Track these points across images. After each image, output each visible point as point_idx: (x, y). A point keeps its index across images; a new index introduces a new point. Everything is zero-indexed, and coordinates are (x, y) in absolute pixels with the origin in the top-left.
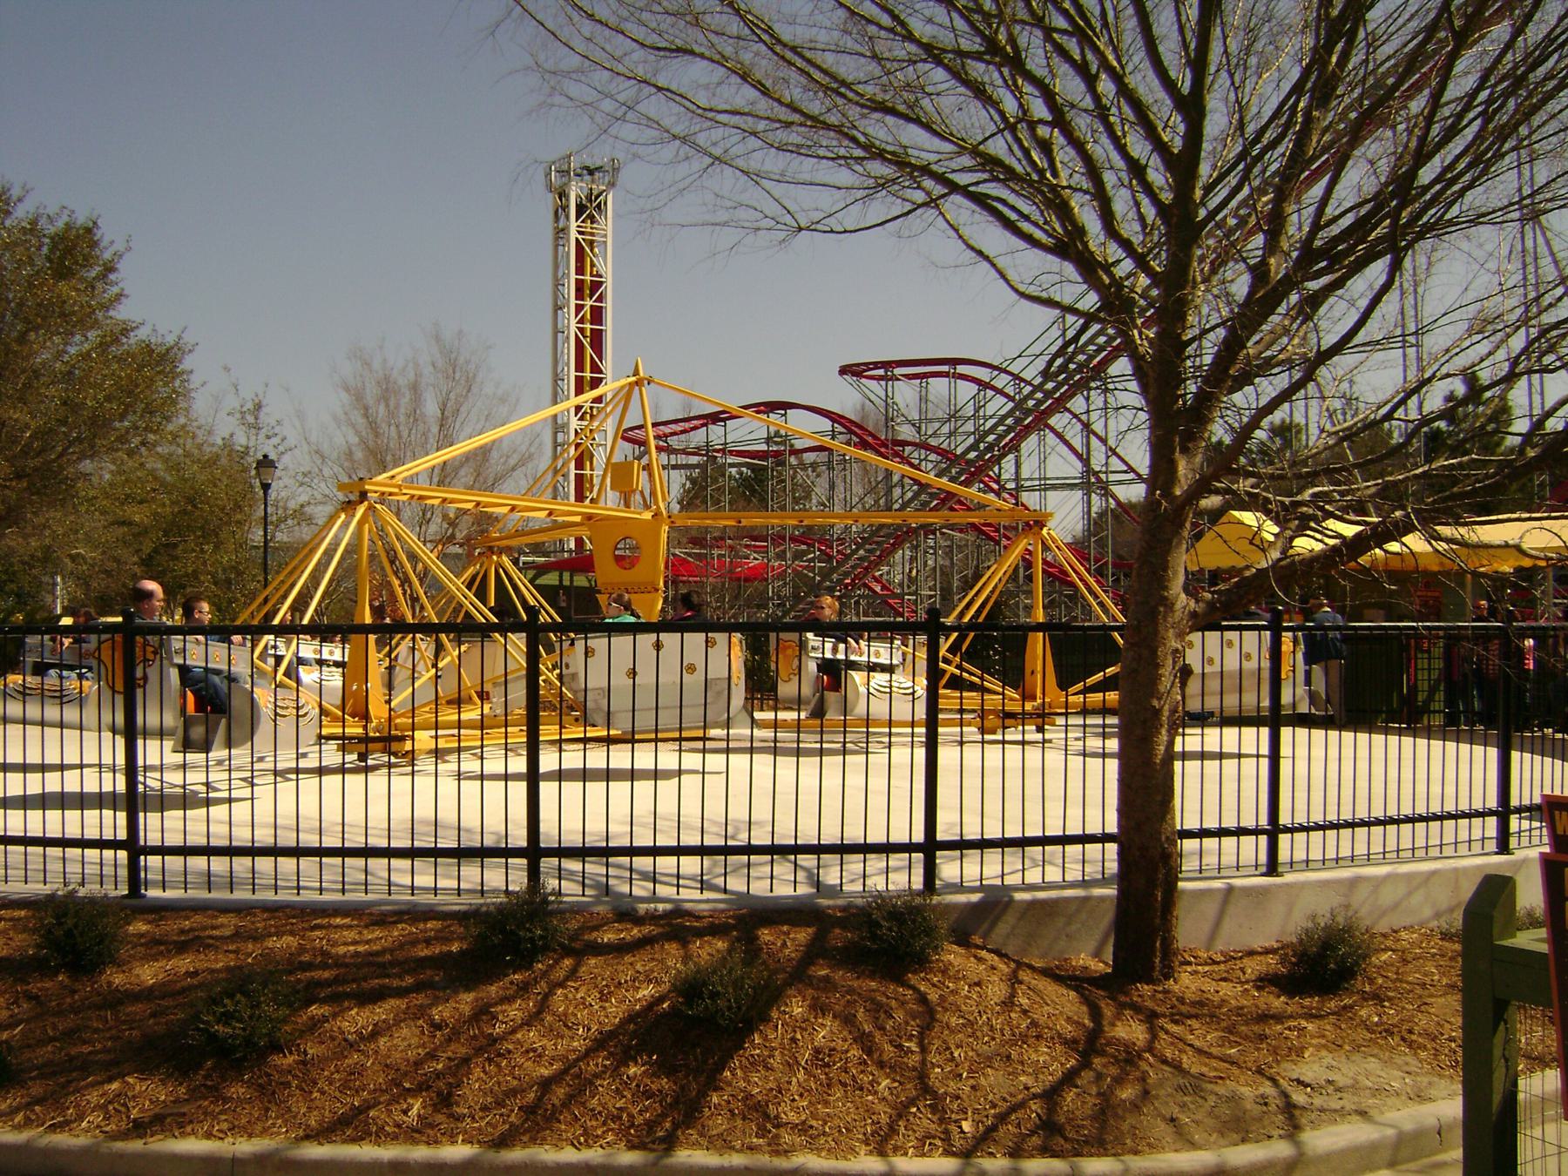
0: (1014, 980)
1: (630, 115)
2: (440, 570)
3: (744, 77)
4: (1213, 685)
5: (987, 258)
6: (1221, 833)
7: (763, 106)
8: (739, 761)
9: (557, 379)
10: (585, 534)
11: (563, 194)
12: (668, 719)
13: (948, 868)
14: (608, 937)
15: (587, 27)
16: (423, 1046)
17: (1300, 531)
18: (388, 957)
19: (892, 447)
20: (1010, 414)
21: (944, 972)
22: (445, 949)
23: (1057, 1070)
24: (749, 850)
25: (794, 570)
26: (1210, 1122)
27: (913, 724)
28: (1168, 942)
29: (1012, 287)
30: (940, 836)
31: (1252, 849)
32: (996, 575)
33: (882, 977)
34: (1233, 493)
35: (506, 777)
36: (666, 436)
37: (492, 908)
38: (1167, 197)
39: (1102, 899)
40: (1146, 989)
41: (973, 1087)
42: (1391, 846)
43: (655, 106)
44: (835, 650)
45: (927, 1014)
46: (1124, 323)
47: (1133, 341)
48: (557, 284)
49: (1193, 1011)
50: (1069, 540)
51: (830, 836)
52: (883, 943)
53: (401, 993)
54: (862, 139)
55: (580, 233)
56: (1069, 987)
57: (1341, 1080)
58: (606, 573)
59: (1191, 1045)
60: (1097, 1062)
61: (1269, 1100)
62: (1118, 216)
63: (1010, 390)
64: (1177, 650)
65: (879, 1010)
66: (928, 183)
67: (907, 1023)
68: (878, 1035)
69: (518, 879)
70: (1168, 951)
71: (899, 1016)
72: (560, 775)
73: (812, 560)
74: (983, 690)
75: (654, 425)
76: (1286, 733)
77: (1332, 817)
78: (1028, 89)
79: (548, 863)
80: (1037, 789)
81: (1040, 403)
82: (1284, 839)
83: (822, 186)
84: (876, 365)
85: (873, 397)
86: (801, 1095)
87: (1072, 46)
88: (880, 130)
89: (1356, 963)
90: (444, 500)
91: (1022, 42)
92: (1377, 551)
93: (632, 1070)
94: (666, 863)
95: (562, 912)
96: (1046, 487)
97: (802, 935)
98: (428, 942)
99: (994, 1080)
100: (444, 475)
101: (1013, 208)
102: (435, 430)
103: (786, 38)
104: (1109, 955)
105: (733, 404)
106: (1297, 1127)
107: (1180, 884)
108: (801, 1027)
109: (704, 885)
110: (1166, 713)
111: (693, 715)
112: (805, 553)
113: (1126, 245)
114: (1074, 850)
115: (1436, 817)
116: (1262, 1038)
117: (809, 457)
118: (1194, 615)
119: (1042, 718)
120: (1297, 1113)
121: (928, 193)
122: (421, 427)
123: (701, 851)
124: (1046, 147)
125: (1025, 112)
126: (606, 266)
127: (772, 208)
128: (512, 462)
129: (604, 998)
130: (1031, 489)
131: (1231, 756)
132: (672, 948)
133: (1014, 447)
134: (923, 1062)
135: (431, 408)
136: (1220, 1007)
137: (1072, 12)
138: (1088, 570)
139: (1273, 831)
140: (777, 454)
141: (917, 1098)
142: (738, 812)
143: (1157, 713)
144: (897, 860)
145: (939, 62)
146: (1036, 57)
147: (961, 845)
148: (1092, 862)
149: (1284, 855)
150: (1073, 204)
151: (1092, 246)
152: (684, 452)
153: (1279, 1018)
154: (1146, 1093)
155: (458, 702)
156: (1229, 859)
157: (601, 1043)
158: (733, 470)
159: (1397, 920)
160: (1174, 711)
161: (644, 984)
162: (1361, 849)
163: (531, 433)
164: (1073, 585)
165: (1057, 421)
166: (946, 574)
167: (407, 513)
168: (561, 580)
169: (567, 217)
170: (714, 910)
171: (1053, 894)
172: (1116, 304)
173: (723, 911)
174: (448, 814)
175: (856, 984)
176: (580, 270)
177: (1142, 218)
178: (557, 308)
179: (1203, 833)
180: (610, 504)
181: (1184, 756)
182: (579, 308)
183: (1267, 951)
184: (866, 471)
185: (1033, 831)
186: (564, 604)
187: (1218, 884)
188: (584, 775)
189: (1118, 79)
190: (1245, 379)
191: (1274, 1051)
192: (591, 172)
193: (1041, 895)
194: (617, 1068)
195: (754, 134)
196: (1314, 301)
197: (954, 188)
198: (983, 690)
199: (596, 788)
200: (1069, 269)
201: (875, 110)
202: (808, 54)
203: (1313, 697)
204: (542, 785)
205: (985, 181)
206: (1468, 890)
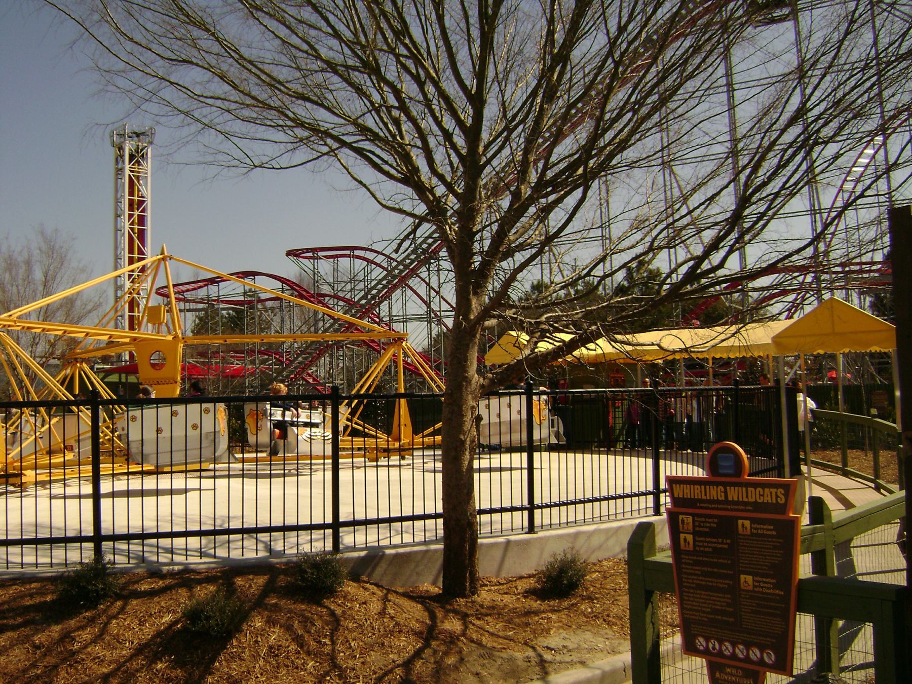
0: (385, 600)
1: (154, 99)
2: (42, 373)
3: (222, 77)
4: (505, 428)
5: (365, 186)
6: (502, 510)
7: (234, 95)
8: (222, 483)
9: (117, 258)
10: (133, 349)
11: (121, 148)
12: (179, 457)
13: (347, 538)
14: (144, 587)
15: (129, 46)
16: (28, 660)
17: (542, 338)
18: (6, 606)
19: (319, 298)
20: (384, 278)
21: (345, 597)
22: (42, 599)
23: (411, 650)
24: (229, 532)
25: (261, 371)
26: (498, 673)
27: (324, 458)
28: (473, 574)
29: (378, 202)
30: (342, 519)
31: (520, 519)
32: (377, 369)
33: (309, 603)
34: (503, 317)
35: (80, 497)
36: (183, 292)
37: (72, 573)
38: (464, 152)
39: (436, 551)
40: (462, 601)
41: (363, 663)
42: (597, 514)
43: (169, 93)
44: (283, 415)
45: (335, 622)
46: (441, 222)
47: (446, 232)
48: (117, 201)
49: (489, 612)
50: (420, 350)
51: (277, 522)
52: (308, 583)
53: (14, 628)
54: (291, 115)
55: (131, 171)
56: (417, 602)
57: (571, 646)
58: (145, 372)
59: (488, 631)
60: (434, 644)
61: (532, 659)
62: (437, 162)
63: (385, 265)
64: (473, 407)
65: (306, 621)
66: (329, 141)
67: (323, 628)
68: (306, 636)
69: (87, 553)
70: (474, 579)
71: (319, 624)
72: (113, 495)
73: (271, 364)
74: (366, 435)
75: (174, 286)
76: (536, 455)
77: (563, 499)
78: (386, 88)
79: (106, 545)
80: (397, 491)
81: (401, 271)
82: (537, 512)
83: (270, 143)
84: (308, 250)
85: (306, 269)
86: (262, 674)
87: (410, 64)
88: (302, 110)
89: (578, 580)
90: (44, 329)
91: (382, 62)
92: (583, 348)
93: (159, 666)
94: (179, 542)
95: (115, 574)
96: (406, 320)
97: (261, 580)
98: (31, 596)
99: (375, 658)
100: (47, 314)
101: (378, 156)
102: (41, 288)
103: (246, 56)
104: (441, 585)
105: (224, 273)
106: (547, 673)
107: (479, 540)
108: (261, 633)
109: (202, 554)
110: (468, 443)
111: (193, 454)
112: (267, 360)
113: (441, 178)
114: (419, 524)
115: (628, 496)
116: (527, 624)
117: (269, 304)
118: (482, 386)
119: (402, 452)
120: (547, 665)
121: (330, 148)
122: (32, 286)
123: (200, 533)
124: (397, 122)
125: (385, 102)
126: (147, 191)
127: (238, 154)
128: (89, 308)
129: (141, 623)
130: (398, 321)
131: (506, 469)
132: (183, 592)
133: (388, 296)
134: (333, 650)
135: (38, 275)
136: (503, 609)
137: (410, 45)
138: (430, 367)
139: (531, 508)
140: (250, 302)
141: (330, 671)
142: (222, 511)
143: (463, 443)
144: (317, 534)
145: (336, 72)
146: (391, 71)
147: (354, 523)
148: (430, 530)
149: (537, 522)
150: (412, 154)
151: (423, 178)
152: (194, 301)
153: (536, 613)
154: (462, 659)
155: (50, 453)
156: (507, 525)
157: (139, 651)
158: (224, 312)
159: (600, 555)
160: (472, 441)
161: (165, 615)
162: (580, 517)
163: (100, 290)
164: (422, 375)
165: (414, 282)
166: (350, 371)
167: (23, 340)
168: (120, 379)
169: (124, 162)
170: (208, 569)
171: (408, 549)
172: (436, 211)
173: (214, 569)
174: (43, 518)
175: (293, 607)
176: (131, 193)
177: (451, 164)
178: (117, 216)
179: (492, 511)
180: (150, 332)
181: (480, 470)
182: (131, 216)
183: (530, 576)
184: (303, 313)
185: (395, 514)
186: (122, 394)
187: (501, 540)
188: (128, 494)
189: (436, 84)
190: (510, 253)
191: (534, 632)
192: (138, 135)
193: (401, 550)
194: (150, 665)
195: (228, 111)
196: (547, 210)
197: (344, 144)
198: (376, 437)
199: (135, 501)
200: (409, 191)
201: (297, 98)
202: (260, 66)
203: (557, 435)
204: (102, 500)
205: (362, 140)
206: (625, 539)
